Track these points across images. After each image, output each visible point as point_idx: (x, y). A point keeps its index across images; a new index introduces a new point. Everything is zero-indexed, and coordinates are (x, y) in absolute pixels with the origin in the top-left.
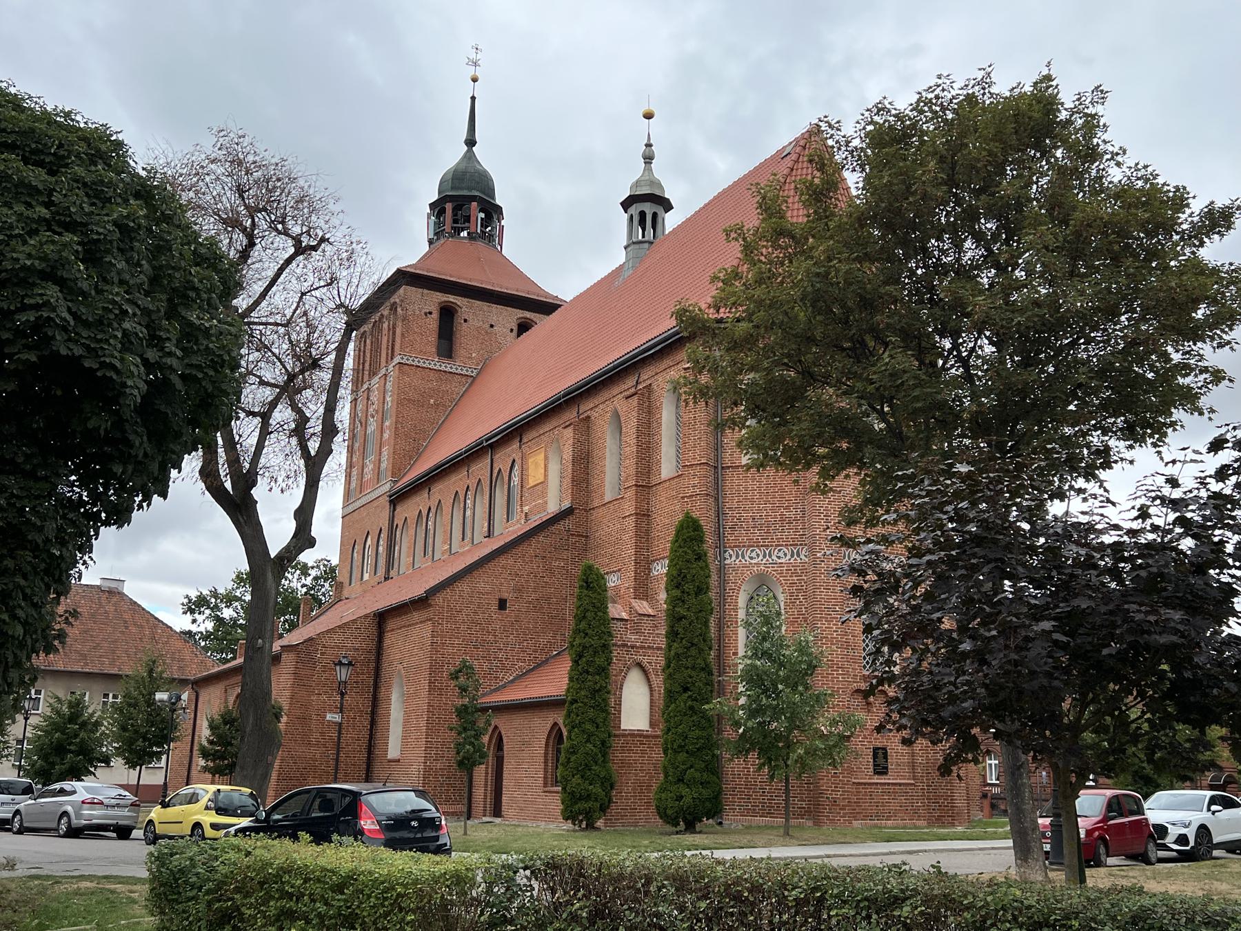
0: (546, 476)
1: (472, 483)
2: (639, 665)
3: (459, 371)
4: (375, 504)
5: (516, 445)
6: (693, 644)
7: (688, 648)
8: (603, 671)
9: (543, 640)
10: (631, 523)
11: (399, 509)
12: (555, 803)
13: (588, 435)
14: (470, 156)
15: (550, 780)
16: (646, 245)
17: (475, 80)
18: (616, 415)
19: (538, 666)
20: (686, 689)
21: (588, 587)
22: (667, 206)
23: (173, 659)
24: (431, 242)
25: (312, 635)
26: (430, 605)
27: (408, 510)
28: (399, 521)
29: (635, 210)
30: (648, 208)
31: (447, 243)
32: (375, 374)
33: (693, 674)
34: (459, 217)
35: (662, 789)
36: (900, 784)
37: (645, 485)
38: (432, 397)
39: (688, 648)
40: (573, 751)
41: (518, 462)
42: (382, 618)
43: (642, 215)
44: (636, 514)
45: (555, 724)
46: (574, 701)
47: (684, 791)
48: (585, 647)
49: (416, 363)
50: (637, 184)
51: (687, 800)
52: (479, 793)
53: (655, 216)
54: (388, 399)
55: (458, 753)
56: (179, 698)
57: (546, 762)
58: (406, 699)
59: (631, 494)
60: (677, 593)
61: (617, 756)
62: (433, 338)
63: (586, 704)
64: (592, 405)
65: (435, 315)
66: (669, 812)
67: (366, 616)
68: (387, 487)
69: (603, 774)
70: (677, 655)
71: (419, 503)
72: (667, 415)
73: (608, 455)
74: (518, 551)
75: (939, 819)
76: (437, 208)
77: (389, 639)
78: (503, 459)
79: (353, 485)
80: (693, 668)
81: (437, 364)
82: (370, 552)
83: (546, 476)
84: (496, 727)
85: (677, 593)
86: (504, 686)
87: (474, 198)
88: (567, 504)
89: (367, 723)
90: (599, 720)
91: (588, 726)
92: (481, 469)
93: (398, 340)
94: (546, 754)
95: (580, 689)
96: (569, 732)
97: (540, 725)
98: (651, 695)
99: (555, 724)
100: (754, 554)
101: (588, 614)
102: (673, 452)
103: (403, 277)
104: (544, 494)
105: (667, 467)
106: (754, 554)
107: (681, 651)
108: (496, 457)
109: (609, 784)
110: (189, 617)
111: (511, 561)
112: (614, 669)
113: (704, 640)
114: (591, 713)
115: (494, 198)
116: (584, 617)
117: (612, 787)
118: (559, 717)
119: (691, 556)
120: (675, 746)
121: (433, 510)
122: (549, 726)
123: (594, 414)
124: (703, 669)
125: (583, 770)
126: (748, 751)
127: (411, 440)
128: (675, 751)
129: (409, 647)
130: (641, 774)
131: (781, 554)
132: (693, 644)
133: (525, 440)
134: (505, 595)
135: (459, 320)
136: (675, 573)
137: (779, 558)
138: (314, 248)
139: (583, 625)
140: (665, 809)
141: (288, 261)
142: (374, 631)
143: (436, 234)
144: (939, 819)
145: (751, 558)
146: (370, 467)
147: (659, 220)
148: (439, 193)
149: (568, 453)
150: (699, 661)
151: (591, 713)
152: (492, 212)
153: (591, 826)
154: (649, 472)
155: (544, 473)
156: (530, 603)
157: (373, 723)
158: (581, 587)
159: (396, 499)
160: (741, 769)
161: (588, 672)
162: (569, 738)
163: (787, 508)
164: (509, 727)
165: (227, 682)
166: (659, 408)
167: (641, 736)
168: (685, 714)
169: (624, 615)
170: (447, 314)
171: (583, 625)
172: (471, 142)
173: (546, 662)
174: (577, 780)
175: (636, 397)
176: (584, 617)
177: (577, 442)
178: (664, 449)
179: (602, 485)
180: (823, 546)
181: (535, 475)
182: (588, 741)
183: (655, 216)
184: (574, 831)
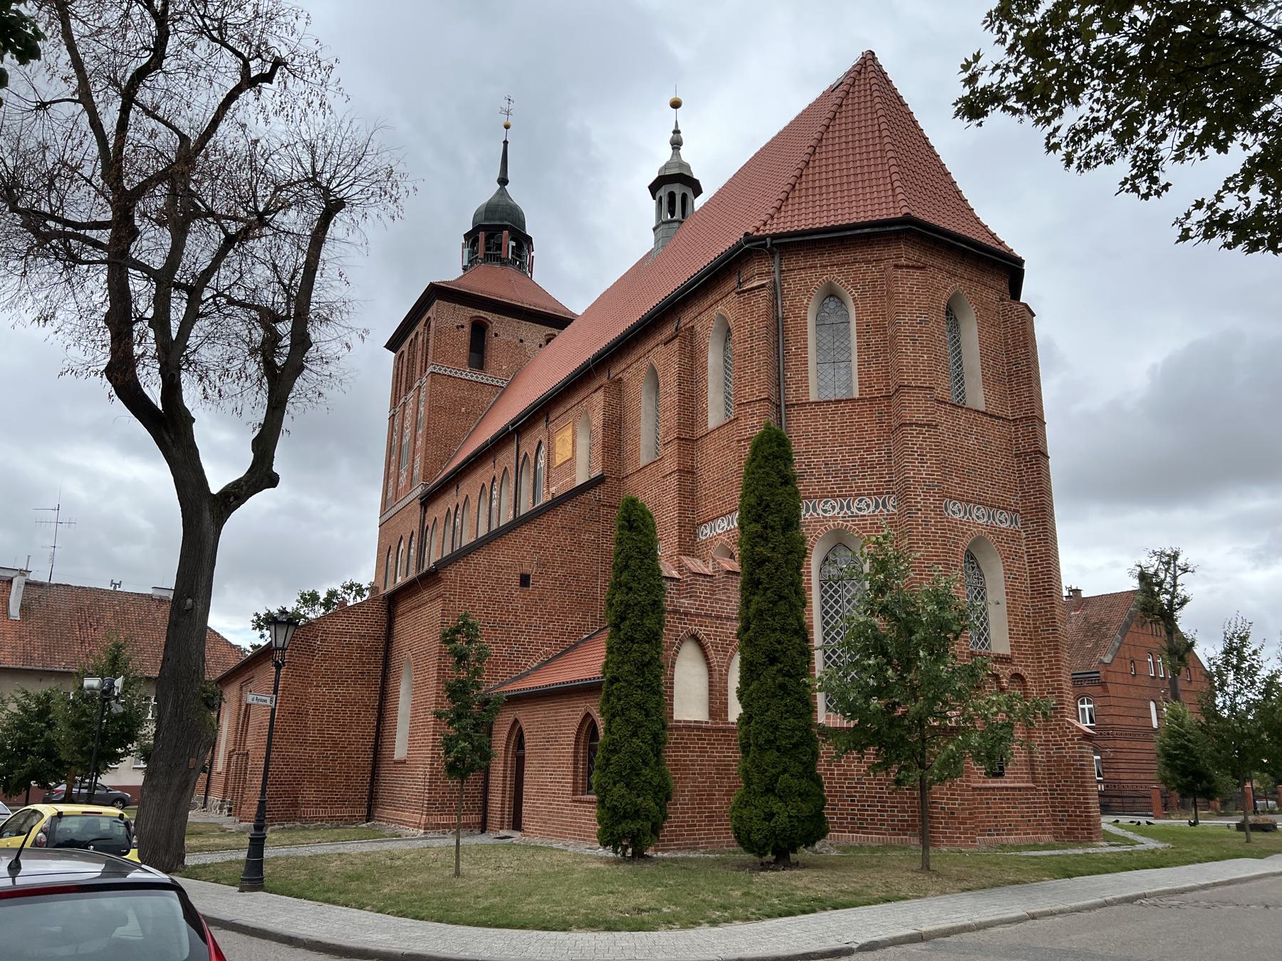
0: (574, 451)
1: (498, 472)
2: (695, 638)
4: (409, 507)
5: (542, 426)
6: (781, 598)
7: (774, 603)
8: (653, 637)
9: (570, 622)
10: (673, 481)
11: (429, 510)
12: (588, 816)
13: (621, 398)
14: (502, 192)
15: (583, 785)
16: (676, 225)
17: (507, 127)
18: (653, 372)
19: (566, 651)
20: (773, 661)
21: (631, 528)
22: (697, 190)
23: (217, 663)
24: (465, 269)
26: (440, 580)
27: (437, 511)
28: (429, 522)
29: (663, 192)
30: (678, 189)
31: (482, 268)
32: (410, 388)
33: (783, 637)
35: (744, 803)
36: (1020, 789)
37: (688, 437)
38: (463, 405)
39: (774, 603)
40: (613, 749)
41: (545, 442)
43: (672, 196)
44: (679, 470)
45: (588, 715)
46: (613, 680)
47: (776, 806)
48: (628, 606)
49: (448, 373)
50: (666, 167)
51: (782, 820)
52: (496, 800)
53: (684, 197)
54: (422, 409)
55: (447, 752)
56: (112, 686)
57: (576, 763)
58: (416, 688)
59: (672, 449)
60: (756, 527)
61: (669, 755)
62: (465, 350)
63: (630, 683)
64: (624, 366)
65: (467, 329)
66: (755, 837)
68: (418, 491)
69: (656, 781)
70: (760, 613)
72: (713, 358)
73: (643, 416)
74: (544, 520)
75: (1070, 832)
76: (471, 238)
77: (401, 624)
78: (528, 444)
79: (390, 494)
80: (783, 630)
82: (403, 557)
83: (574, 451)
84: (516, 721)
85: (756, 527)
86: (527, 674)
87: (505, 227)
88: (597, 472)
89: (373, 719)
90: (650, 705)
91: (635, 714)
92: (507, 458)
93: (431, 351)
94: (576, 753)
95: (623, 662)
96: (609, 722)
97: (569, 717)
98: (711, 676)
99: (588, 715)
101: (632, 563)
102: (721, 398)
103: (436, 292)
104: (572, 470)
105: (714, 416)
107: (765, 606)
108: (522, 442)
109: (663, 794)
110: (258, 633)
111: (534, 533)
112: (667, 637)
113: (797, 593)
114: (638, 696)
115: (524, 228)
116: (626, 567)
117: (668, 799)
118: (593, 707)
119: (774, 478)
120: (761, 741)
121: (461, 507)
122: (579, 718)
123: (626, 376)
124: (796, 632)
125: (629, 776)
126: (866, 746)
127: (440, 442)
128: (761, 748)
129: (420, 631)
130: (706, 785)
131: (863, 505)
132: (781, 598)
133: (552, 418)
134: (526, 570)
135: (490, 333)
136: (753, 501)
137: (860, 509)
138: (268, 78)
139: (624, 577)
140: (749, 833)
141: (232, 96)
142: (383, 615)
143: (470, 262)
144: (1070, 832)
145: (825, 511)
146: (404, 474)
147: (689, 201)
149: (597, 419)
150: (791, 620)
151: (638, 696)
152: (523, 242)
153: (639, 855)
154: (693, 424)
155: (572, 450)
156: (556, 579)
157: (381, 718)
158: (621, 527)
159: (428, 500)
160: (846, 773)
161: (633, 640)
162: (608, 730)
163: (868, 450)
164: (533, 720)
165: (242, 680)
166: (704, 352)
167: (698, 729)
168: (774, 695)
169: (675, 574)
170: (479, 329)
171: (624, 577)
172: (503, 181)
173: (574, 647)
174: (619, 789)
175: (676, 341)
176: (626, 567)
177: (608, 405)
178: (711, 396)
179: (636, 450)
180: (919, 491)
181: (562, 452)
182: (635, 734)
183: (684, 197)
184: (617, 862)
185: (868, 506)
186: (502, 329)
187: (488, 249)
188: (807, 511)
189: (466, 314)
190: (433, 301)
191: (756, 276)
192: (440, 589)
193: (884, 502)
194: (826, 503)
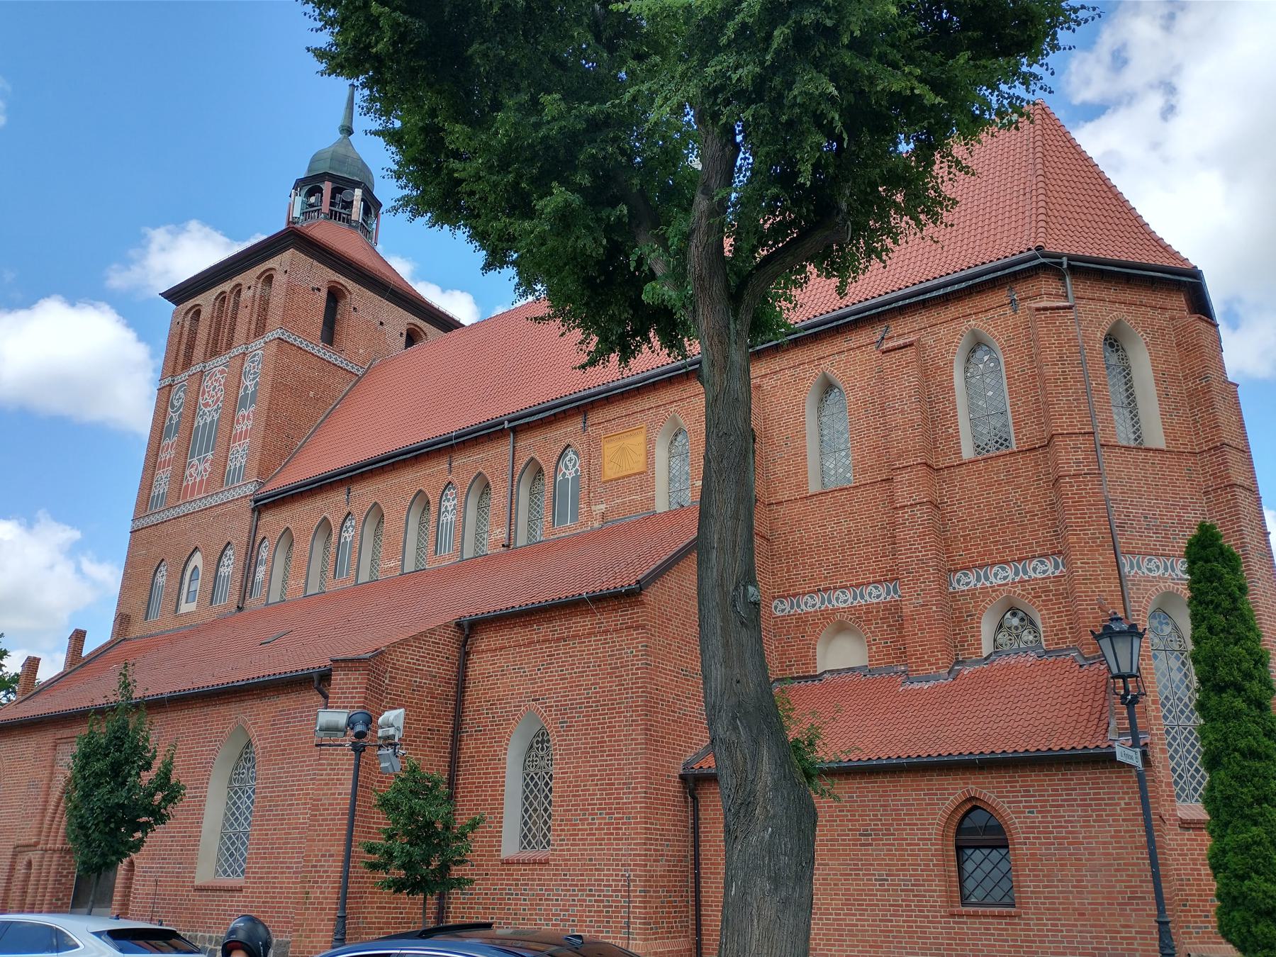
3: (343, 365)
4: (219, 511)
25: (382, 644)
27: (274, 521)
34: (337, 200)
42: (470, 630)
65: (324, 294)
67: (446, 626)
68: (250, 489)
71: (303, 516)
77: (480, 665)
81: (320, 350)
100: (1152, 566)
106: (1152, 566)
142: (452, 650)
148: (309, 170)
159: (264, 505)
185: (1158, 567)
186: (363, 304)
187: (332, 204)
188: (1132, 567)
189: (326, 275)
190: (285, 249)
191: (1045, 293)
192: (638, 614)
193: (986, 573)
194: (1150, 561)
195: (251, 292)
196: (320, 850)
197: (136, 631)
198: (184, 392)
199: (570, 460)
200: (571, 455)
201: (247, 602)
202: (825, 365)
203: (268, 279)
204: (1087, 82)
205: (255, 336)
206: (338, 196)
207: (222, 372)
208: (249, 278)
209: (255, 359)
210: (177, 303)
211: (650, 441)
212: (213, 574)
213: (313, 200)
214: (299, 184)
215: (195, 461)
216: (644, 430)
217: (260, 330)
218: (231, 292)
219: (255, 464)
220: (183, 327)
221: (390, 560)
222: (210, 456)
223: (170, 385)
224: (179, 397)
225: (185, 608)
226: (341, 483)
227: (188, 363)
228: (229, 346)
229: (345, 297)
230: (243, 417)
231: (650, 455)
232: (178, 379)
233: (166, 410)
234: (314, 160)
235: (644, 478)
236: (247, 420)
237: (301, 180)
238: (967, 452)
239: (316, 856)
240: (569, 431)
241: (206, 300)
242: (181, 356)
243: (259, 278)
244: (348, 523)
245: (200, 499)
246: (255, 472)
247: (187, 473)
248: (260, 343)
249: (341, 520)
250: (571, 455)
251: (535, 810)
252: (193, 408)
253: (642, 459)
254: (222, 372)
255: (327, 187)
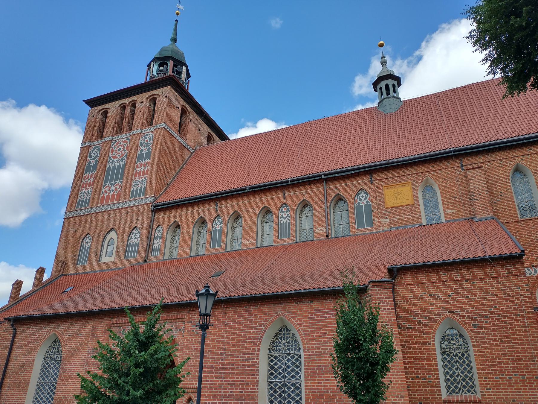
4: (128, 210)
34: (175, 70)
65: (180, 110)
68: (150, 200)
159: (158, 209)
195: (143, 105)
196: (394, 393)
197: (70, 270)
198: (99, 150)
199: (363, 196)
200: (362, 194)
201: (150, 258)
202: (518, 160)
203: (154, 100)
204: (361, 87)
205: (146, 126)
206: (175, 68)
207: (125, 142)
208: (142, 99)
209: (147, 138)
210: (92, 107)
211: (414, 190)
212: (126, 242)
213: (162, 68)
214: (155, 60)
215: (108, 184)
216: (411, 183)
217: (151, 122)
218: (129, 104)
219: (152, 188)
220: (96, 118)
221: (249, 240)
222: (119, 182)
223: (89, 146)
224: (94, 153)
225: (104, 260)
226: (212, 200)
227: (101, 135)
228: (130, 129)
229: (187, 114)
230: (141, 165)
231: (415, 196)
232: (94, 143)
233: (87, 158)
234: (162, 50)
235: (413, 207)
236: (143, 166)
237: (157, 58)
238: (443, 220)
239: (393, 397)
240: (362, 182)
241: (113, 107)
242: (95, 133)
243: (147, 98)
244: (217, 221)
245: (114, 204)
246: (153, 192)
247: (103, 190)
248: (151, 129)
249: (213, 219)
250: (362, 194)
251: (48, 394)
252: (106, 158)
253: (410, 198)
254: (125, 142)
255: (170, 64)
